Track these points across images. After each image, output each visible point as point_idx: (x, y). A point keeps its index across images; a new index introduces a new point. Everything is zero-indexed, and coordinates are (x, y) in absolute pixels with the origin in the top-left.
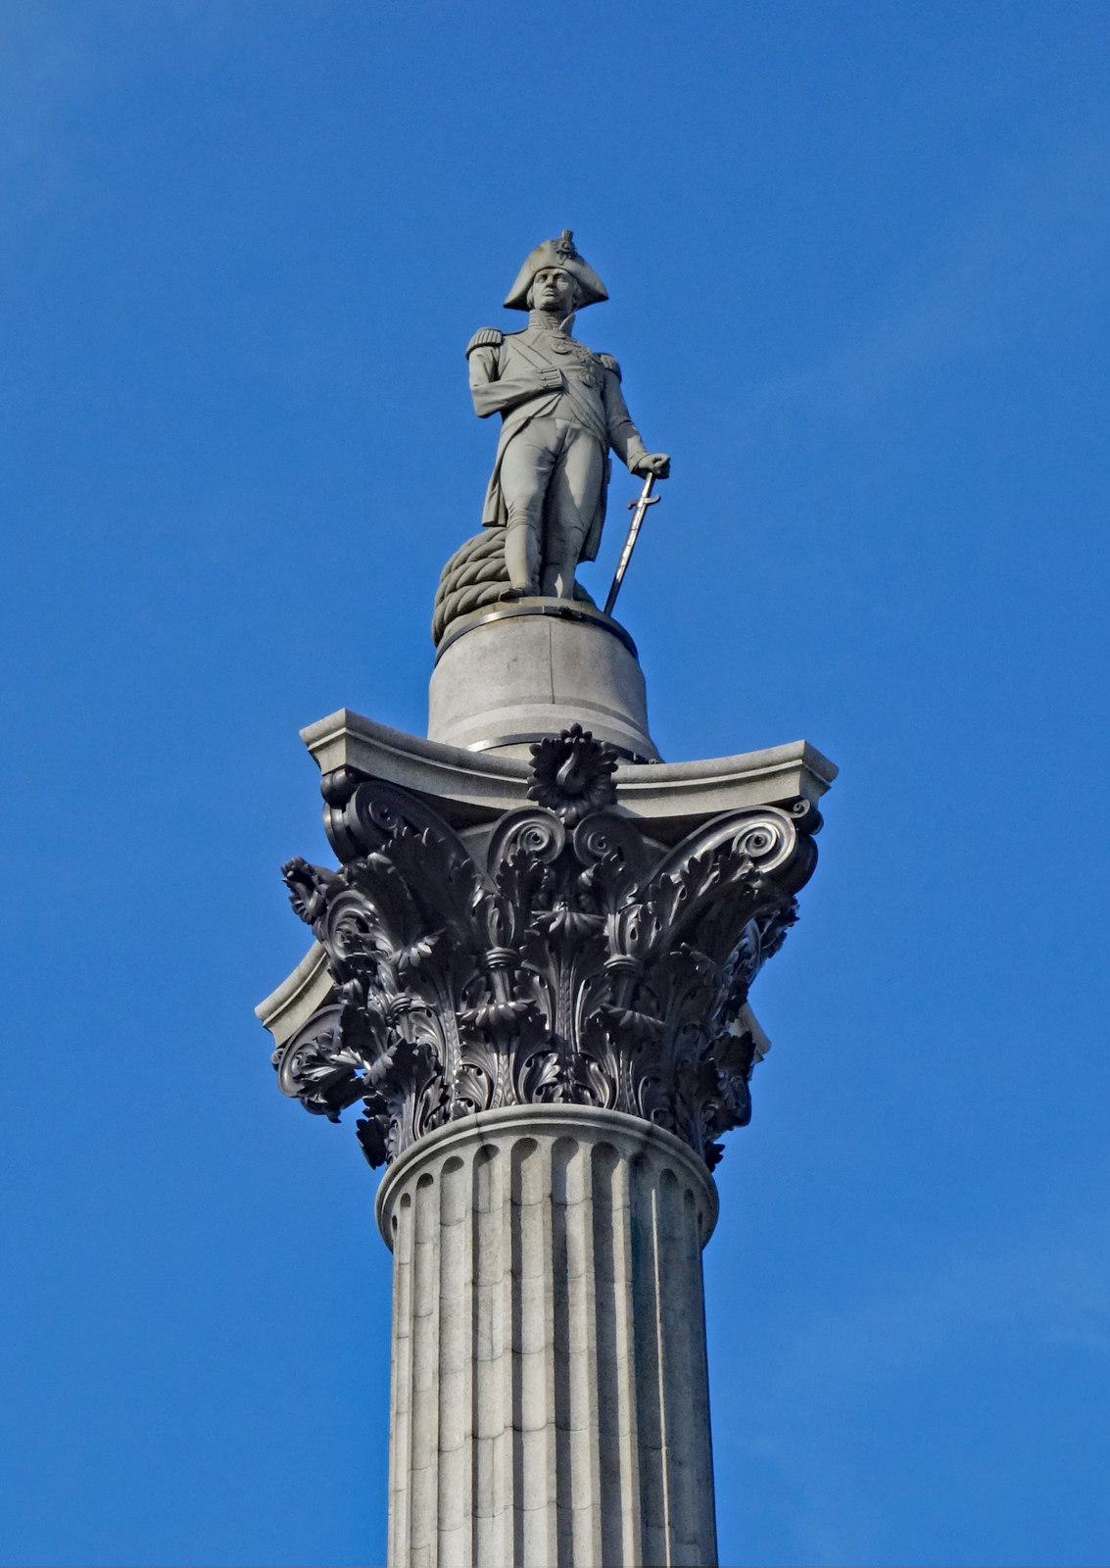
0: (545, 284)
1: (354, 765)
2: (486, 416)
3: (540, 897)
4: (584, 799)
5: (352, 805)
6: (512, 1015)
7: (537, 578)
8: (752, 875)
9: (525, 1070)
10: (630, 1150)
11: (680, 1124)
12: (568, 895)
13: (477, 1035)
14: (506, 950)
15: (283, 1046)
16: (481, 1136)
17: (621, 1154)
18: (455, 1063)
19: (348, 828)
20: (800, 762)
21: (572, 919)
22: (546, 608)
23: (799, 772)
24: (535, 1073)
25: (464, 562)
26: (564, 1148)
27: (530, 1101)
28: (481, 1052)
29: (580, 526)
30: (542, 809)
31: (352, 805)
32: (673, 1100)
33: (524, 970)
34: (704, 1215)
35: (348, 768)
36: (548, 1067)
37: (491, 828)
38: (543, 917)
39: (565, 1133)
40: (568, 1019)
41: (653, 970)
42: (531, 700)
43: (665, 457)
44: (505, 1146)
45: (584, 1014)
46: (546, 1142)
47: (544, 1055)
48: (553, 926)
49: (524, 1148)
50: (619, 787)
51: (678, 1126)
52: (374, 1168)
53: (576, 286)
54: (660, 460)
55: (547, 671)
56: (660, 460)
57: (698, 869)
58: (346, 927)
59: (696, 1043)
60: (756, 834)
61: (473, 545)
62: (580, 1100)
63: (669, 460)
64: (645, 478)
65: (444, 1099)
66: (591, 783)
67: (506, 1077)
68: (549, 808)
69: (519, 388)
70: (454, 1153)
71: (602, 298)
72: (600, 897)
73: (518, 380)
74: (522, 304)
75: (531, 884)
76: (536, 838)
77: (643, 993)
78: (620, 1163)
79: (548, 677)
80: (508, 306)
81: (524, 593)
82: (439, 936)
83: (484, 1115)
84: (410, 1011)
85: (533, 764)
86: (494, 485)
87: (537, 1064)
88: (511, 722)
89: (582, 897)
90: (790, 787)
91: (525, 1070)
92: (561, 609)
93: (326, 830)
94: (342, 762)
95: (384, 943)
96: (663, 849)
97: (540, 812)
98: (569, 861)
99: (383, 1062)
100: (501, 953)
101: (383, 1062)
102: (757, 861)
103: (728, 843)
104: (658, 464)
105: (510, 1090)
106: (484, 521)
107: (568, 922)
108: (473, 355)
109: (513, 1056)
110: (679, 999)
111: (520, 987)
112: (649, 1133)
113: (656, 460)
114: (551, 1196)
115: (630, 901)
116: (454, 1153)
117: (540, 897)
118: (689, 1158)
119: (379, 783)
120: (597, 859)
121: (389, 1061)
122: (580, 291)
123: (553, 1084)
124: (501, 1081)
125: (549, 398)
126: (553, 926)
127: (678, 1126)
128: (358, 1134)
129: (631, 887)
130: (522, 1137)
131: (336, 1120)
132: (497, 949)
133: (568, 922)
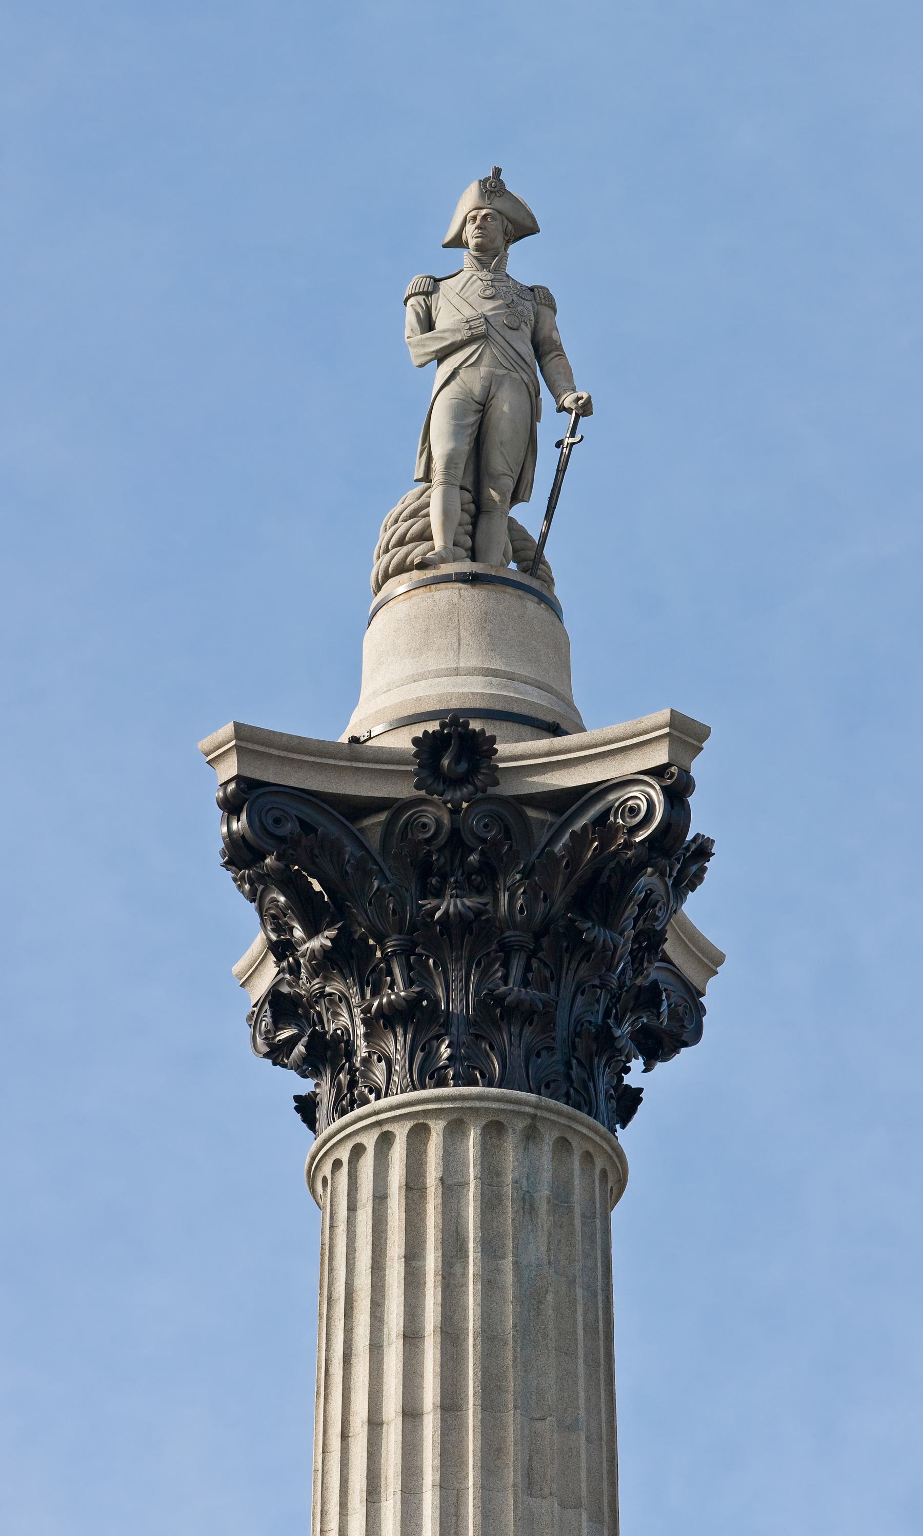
0: (475, 226)
1: (247, 774)
2: (421, 366)
3: (434, 881)
4: (469, 783)
5: (244, 817)
6: (404, 1003)
7: (472, 506)
8: (628, 845)
9: (419, 1055)
10: (520, 1124)
11: (575, 1089)
12: (460, 878)
13: (380, 1022)
14: (401, 937)
15: (255, 1006)
16: (379, 1123)
17: (510, 1130)
18: (362, 1049)
19: (243, 837)
20: (667, 730)
21: (455, 905)
22: (456, 574)
23: (667, 740)
24: (431, 1054)
25: (396, 522)
26: (455, 1130)
27: (424, 1087)
28: (377, 1041)
29: (509, 473)
30: (429, 797)
31: (244, 817)
32: (569, 1066)
33: (421, 955)
34: (608, 1169)
35: (237, 778)
36: (443, 1047)
37: (383, 817)
38: (429, 906)
39: (455, 1116)
40: (462, 1000)
41: (545, 942)
42: (439, 674)
43: (585, 396)
44: (401, 1132)
45: (476, 994)
46: (437, 1128)
47: (439, 1038)
48: (437, 915)
49: (419, 1134)
50: (501, 765)
51: (572, 1091)
52: (297, 1098)
53: (506, 221)
54: (582, 398)
55: (455, 640)
56: (582, 398)
57: (580, 840)
58: (272, 912)
59: (598, 1001)
60: (630, 803)
61: (406, 503)
62: (473, 1083)
63: (589, 398)
64: (571, 414)
65: (353, 1084)
66: (474, 770)
67: (402, 1063)
68: (435, 796)
69: (446, 339)
70: (386, 1128)
71: (533, 230)
72: (486, 878)
73: (444, 331)
74: (458, 242)
75: (425, 870)
76: (424, 825)
77: (535, 964)
78: (510, 1139)
79: (455, 646)
80: (445, 246)
81: (443, 560)
82: (338, 929)
83: (383, 1102)
84: (326, 996)
85: (416, 755)
86: (423, 444)
87: (430, 1046)
88: (418, 699)
89: (473, 877)
90: (659, 756)
91: (419, 1055)
92: (471, 574)
93: (224, 839)
94: (234, 772)
95: (298, 933)
96: (548, 817)
97: (426, 800)
98: (456, 841)
99: (299, 1051)
100: (404, 940)
101: (299, 1051)
102: (633, 830)
103: (606, 813)
104: (580, 402)
105: (405, 1077)
106: (417, 362)
107: (452, 909)
108: (412, 301)
109: (409, 1036)
110: (574, 965)
111: (416, 974)
112: (537, 1106)
113: (578, 399)
114: (441, 1179)
115: (518, 877)
116: (386, 1128)
117: (434, 881)
118: (582, 1124)
119: (275, 789)
120: (484, 841)
121: (303, 1049)
122: (510, 227)
123: (445, 1067)
124: (397, 1068)
125: (474, 347)
126: (437, 915)
127: (572, 1091)
128: (296, 1108)
129: (517, 864)
130: (416, 1122)
131: (498, 172)
132: (395, 936)
133: (452, 909)
